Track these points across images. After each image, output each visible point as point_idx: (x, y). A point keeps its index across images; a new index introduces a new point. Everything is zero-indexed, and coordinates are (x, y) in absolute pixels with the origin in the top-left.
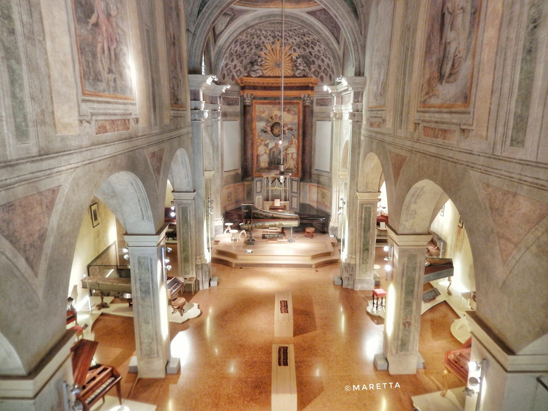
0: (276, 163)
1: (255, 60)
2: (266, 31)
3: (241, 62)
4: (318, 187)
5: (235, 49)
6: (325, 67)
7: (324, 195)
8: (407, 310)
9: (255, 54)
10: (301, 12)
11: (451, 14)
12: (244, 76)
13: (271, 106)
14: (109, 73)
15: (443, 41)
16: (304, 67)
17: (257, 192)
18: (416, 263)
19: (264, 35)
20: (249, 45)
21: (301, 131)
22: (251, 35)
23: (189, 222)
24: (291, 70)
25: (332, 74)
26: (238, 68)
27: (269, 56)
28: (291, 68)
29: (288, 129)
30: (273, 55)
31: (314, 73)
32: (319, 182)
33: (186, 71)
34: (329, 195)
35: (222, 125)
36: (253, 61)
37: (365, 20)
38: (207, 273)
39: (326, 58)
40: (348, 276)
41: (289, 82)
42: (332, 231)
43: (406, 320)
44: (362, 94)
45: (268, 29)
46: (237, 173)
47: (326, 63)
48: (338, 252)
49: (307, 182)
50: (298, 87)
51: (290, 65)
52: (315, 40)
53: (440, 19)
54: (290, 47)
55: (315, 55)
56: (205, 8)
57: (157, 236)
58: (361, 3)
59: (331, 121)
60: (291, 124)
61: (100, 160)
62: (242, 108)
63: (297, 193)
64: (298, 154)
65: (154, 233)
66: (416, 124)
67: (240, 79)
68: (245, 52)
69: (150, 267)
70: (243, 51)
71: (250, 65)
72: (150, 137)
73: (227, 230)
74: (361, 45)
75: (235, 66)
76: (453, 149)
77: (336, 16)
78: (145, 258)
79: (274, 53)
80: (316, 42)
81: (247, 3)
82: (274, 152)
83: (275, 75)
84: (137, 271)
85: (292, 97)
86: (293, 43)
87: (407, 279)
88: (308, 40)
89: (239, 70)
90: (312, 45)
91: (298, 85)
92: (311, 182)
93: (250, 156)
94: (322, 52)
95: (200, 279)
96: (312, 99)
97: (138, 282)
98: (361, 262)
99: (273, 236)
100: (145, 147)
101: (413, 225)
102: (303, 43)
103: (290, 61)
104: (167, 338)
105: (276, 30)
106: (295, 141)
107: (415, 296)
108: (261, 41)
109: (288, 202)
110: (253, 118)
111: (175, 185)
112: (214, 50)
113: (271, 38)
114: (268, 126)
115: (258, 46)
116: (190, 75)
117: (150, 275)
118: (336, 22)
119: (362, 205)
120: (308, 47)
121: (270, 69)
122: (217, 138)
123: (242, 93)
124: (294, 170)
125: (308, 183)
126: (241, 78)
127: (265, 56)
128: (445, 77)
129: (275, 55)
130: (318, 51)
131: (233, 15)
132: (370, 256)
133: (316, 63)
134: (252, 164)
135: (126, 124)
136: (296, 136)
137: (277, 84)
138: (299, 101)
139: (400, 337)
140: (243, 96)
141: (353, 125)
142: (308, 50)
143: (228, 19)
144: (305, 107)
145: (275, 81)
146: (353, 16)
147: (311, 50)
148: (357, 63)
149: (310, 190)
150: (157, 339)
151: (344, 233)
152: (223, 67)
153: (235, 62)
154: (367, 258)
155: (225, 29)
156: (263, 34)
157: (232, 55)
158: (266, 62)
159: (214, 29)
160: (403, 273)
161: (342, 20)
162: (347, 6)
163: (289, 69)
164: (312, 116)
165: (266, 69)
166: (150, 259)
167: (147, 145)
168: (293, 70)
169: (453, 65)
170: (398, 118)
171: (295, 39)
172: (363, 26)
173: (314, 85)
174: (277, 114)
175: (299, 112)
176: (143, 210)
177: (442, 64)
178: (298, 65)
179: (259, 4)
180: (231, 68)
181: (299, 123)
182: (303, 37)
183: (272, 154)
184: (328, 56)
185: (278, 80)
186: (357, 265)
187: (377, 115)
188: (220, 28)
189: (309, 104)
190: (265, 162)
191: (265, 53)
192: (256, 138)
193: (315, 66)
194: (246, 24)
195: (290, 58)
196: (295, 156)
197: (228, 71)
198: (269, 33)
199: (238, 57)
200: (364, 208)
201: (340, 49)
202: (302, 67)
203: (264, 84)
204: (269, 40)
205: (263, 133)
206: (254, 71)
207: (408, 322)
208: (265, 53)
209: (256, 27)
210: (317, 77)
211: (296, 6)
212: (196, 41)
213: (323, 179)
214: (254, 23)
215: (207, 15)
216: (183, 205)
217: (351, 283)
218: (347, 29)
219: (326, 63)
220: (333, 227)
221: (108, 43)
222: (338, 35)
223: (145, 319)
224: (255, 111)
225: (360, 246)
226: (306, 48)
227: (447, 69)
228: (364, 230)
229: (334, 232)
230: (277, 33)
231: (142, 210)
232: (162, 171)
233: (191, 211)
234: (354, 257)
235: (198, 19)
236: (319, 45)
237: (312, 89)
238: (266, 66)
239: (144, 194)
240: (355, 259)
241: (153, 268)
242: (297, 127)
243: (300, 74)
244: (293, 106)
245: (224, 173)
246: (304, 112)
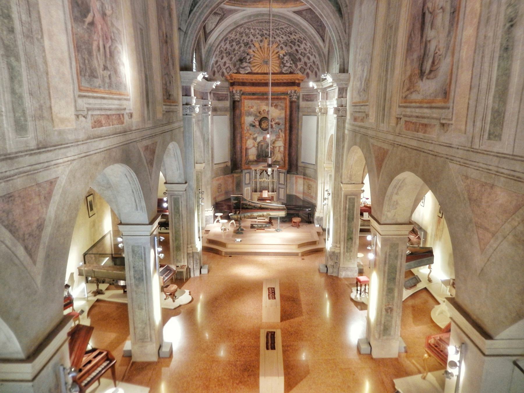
0: (264, 156)
1: (244, 58)
2: (254, 29)
3: (231, 59)
4: (304, 178)
5: (225, 47)
6: (311, 64)
7: (310, 186)
8: (389, 297)
9: (244, 52)
10: (288, 11)
11: (431, 13)
12: (233, 73)
13: (259, 101)
14: (104, 70)
15: (424, 39)
16: (291, 64)
17: (246, 184)
18: (398, 251)
19: (253, 33)
20: (238, 43)
21: (288, 125)
22: (240, 34)
23: (181, 212)
24: (278, 67)
25: (317, 71)
26: (227, 65)
27: (257, 54)
28: (278, 65)
29: (275, 124)
30: (261, 52)
31: (300, 70)
32: (305, 175)
33: (178, 68)
34: (315, 186)
35: (212, 119)
36: (242, 58)
37: (349, 19)
38: (198, 261)
39: (312, 55)
40: (333, 264)
41: (276, 78)
42: (318, 221)
43: (388, 306)
44: (346, 90)
45: (257, 28)
46: (227, 166)
47: (311, 60)
48: (323, 241)
49: (294, 174)
50: (285, 83)
51: (278, 62)
52: (301, 38)
53: (420, 18)
54: (277, 45)
55: (302, 52)
56: (196, 8)
57: (150, 226)
58: (346, 3)
59: (316, 115)
60: (279, 119)
61: (96, 153)
62: (232, 103)
63: (284, 184)
64: (285, 147)
65: (148, 223)
66: (397, 118)
67: (229, 75)
68: (234, 50)
69: (143, 255)
70: (232, 49)
71: (239, 62)
72: (144, 130)
73: (217, 220)
74: (346, 44)
75: (225, 63)
76: (434, 142)
77: (321, 15)
78: (138, 247)
79: (262, 51)
80: (302, 40)
81: (236, 3)
82: (262, 145)
83: (263, 72)
84: (131, 259)
85: (279, 92)
86: (280, 41)
87: (389, 266)
88: (294, 38)
89: (229, 67)
90: (298, 43)
91: (285, 81)
92: (297, 174)
93: (239, 149)
94: (308, 50)
95: (191, 267)
96: (298, 94)
97: (132, 270)
98: (345, 251)
99: (261, 226)
100: (139, 140)
101: (395, 215)
102: (290, 41)
103: (277, 59)
104: (159, 324)
105: (264, 28)
106: (282, 134)
107: (397, 283)
108: (250, 40)
109: (276, 193)
110: (242, 112)
111: (167, 177)
112: (204, 48)
113: (259, 37)
114: (256, 121)
115: (246, 44)
116: (181, 72)
117: (144, 263)
118: (321, 21)
119: (346, 196)
120: (294, 45)
121: (258, 66)
122: (208, 132)
123: (231, 89)
124: (282, 163)
125: (295, 175)
126: (230, 75)
127: (253, 53)
128: (425, 74)
129: (263, 53)
130: (304, 48)
131: (223, 14)
132: (353, 245)
133: (302, 60)
134: (241, 157)
135: (120, 119)
136: (283, 130)
137: (264, 80)
138: (285, 97)
139: (383, 322)
140: (233, 91)
141: (337, 119)
142: (294, 48)
143: (218, 18)
144: (291, 102)
145: (263, 78)
146: (338, 15)
147: (297, 48)
148: (341, 60)
149: (296, 182)
150: (150, 325)
151: (329, 223)
152: (213, 64)
153: (225, 59)
154: (351, 246)
155: (215, 28)
156: (251, 33)
157: (222, 53)
158: (254, 59)
159: (204, 28)
160: (385, 261)
161: (327, 19)
162: (333, 7)
163: (276, 66)
164: (299, 111)
165: (254, 66)
166: (144, 247)
167: (141, 138)
168: (280, 67)
169: (433, 62)
170: (381, 113)
171: (282, 38)
172: (347, 24)
173: (301, 82)
174: (265, 109)
175: (286, 107)
176: (137, 201)
177: (423, 62)
178: (285, 62)
179: (247, 4)
180: (221, 65)
181: (286, 118)
182: (290, 36)
183: (260, 147)
184: (314, 53)
185: (265, 77)
186: (341, 253)
187: (361, 110)
188: (210, 26)
189: (295, 100)
190: (253, 155)
191: (253, 51)
192: (245, 132)
193: (301, 63)
194: (235, 23)
195: (277, 55)
196: (282, 149)
197: (218, 68)
198: (258, 31)
199: (227, 55)
200: (348, 199)
201: (325, 47)
202: (289, 64)
203: (252, 80)
204: (257, 38)
205: (251, 127)
206: (243, 68)
207: (390, 308)
208: (253, 51)
209: (244, 25)
210: (303, 73)
211: (284, 6)
212: (188, 39)
213: (309, 172)
214: (243, 22)
215: (198, 14)
216: (175, 196)
217: (336, 270)
218: (332, 28)
219: (311, 60)
220: (319, 217)
221: (103, 41)
222: (323, 34)
223: (139, 305)
224: (244, 106)
225: (345, 235)
226: (293, 46)
227: (428, 66)
228: (348, 220)
229: (320, 222)
230: (265, 32)
231: (135, 201)
232: (154, 163)
233: (183, 202)
234: (338, 245)
235: (189, 18)
236: (305, 43)
237: (298, 85)
238: (255, 63)
239: (137, 186)
240: (340, 247)
241: (147, 256)
242: (284, 121)
243: (286, 70)
244: (280, 101)
245: (214, 166)
246: (291, 107)
